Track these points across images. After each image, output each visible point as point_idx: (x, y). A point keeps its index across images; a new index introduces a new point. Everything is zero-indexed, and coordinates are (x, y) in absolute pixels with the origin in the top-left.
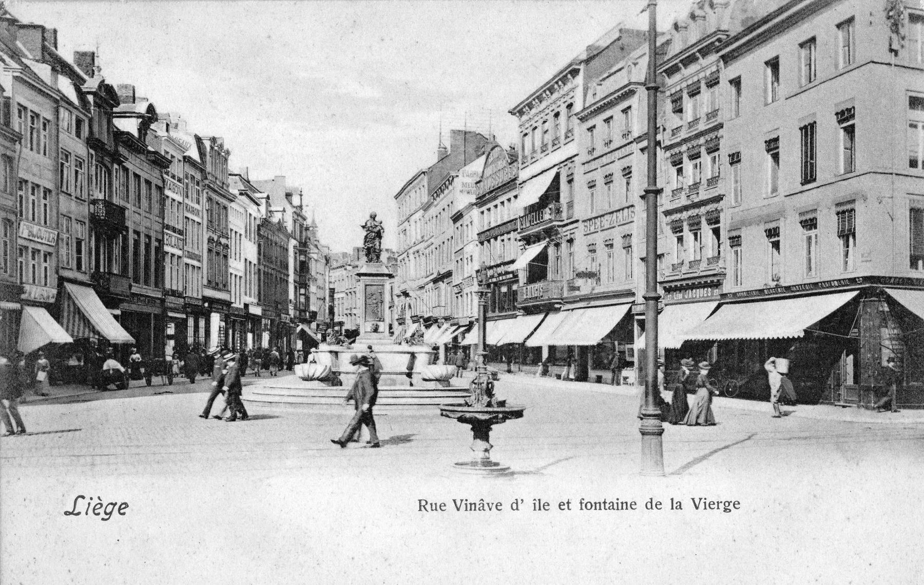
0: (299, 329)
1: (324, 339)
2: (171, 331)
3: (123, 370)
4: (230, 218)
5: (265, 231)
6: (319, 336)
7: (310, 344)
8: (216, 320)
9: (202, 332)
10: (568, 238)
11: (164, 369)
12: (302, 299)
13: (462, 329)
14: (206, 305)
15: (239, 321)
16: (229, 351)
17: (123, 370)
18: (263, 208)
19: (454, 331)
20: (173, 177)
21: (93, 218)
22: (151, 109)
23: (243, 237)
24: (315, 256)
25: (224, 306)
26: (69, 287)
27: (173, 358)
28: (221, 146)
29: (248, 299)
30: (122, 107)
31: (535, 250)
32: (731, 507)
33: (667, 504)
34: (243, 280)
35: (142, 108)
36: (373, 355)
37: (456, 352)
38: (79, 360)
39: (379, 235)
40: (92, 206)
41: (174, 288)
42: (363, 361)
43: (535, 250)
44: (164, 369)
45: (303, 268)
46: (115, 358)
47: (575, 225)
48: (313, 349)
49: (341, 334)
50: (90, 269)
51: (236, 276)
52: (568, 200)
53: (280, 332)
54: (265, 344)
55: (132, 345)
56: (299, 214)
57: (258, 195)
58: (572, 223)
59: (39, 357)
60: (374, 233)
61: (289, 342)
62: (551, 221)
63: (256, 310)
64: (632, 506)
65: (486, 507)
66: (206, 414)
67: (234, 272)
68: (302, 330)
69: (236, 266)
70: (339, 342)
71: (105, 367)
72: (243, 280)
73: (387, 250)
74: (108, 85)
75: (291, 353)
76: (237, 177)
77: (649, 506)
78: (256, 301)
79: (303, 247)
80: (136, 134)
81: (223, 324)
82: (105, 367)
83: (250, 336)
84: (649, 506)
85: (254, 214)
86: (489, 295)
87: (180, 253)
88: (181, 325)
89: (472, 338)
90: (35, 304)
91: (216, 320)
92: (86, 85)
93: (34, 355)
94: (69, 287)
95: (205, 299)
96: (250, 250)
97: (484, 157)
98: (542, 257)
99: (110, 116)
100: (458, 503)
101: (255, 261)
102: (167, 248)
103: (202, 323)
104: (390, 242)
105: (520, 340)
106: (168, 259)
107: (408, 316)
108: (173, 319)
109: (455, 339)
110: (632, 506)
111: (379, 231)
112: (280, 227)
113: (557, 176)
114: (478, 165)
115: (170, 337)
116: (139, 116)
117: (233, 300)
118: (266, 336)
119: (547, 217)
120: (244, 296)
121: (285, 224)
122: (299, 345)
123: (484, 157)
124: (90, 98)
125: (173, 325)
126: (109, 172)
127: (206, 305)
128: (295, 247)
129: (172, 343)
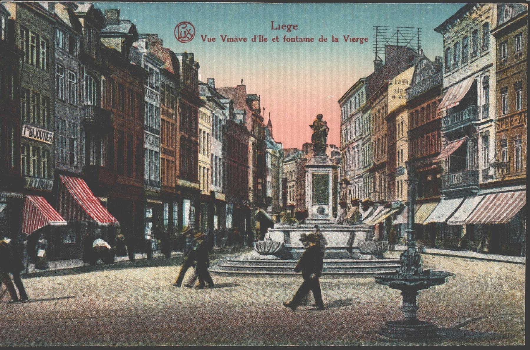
0: (258, 211)
1: (278, 221)
2: (149, 215)
3: (109, 247)
4: (200, 121)
5: (232, 135)
6: (274, 218)
7: (267, 224)
8: (187, 205)
9: (176, 215)
10: (484, 134)
11: (146, 247)
12: (260, 187)
13: (394, 211)
14: (179, 192)
15: (205, 205)
16: (200, 231)
17: (109, 247)
18: (227, 112)
19: (387, 213)
20: (152, 86)
21: (84, 121)
22: (133, 28)
23: (210, 136)
24: (270, 151)
25: (195, 196)
26: (64, 179)
27: (152, 237)
28: (192, 60)
29: (212, 188)
30: (109, 28)
31: (457, 144)
32: (364, 41)
33: (330, 39)
34: (210, 172)
35: (125, 28)
36: (319, 233)
37: (388, 233)
38: (71, 238)
39: (325, 134)
40: (82, 112)
41: (153, 178)
42: (311, 238)
43: (457, 144)
44: (146, 247)
45: (260, 161)
46: (103, 238)
47: (490, 124)
48: (270, 229)
49: (292, 216)
50: (82, 163)
51: (204, 168)
52: (484, 103)
53: (242, 214)
54: (229, 225)
55: (117, 227)
56: (257, 118)
57: (223, 101)
58: (487, 122)
59: (39, 237)
60: (319, 129)
61: (248, 222)
62: (469, 120)
63: (220, 197)
64: (311, 40)
65: (238, 40)
66: (178, 283)
67: (203, 165)
68: (260, 212)
69: (204, 159)
70: (291, 222)
71: (94, 245)
72: (210, 172)
73: (331, 146)
74: (97, 10)
75: (250, 231)
76: (205, 86)
77: (321, 40)
78: (220, 189)
79: (260, 146)
80: (119, 49)
81: (193, 208)
82: (94, 245)
83: (216, 219)
84: (321, 40)
85: (221, 117)
86: (417, 182)
87: (157, 150)
88: (158, 211)
89: (401, 220)
90: (35, 193)
91: (187, 205)
92: (77, 11)
93: (36, 235)
94: (64, 179)
95: (178, 187)
96: (216, 148)
97: (413, 68)
98: (462, 150)
99: (99, 36)
100: (224, 37)
101: (220, 156)
102: (147, 146)
103: (176, 209)
104: (333, 138)
105: (442, 220)
106: (147, 155)
107: (348, 202)
108: (151, 205)
109: (388, 219)
110: (311, 40)
111: (325, 130)
112: (241, 127)
113: (475, 83)
114: (408, 74)
115: (149, 220)
116: (123, 35)
117: (202, 189)
118: (229, 220)
119: (466, 117)
120: (210, 184)
121: (246, 125)
122: (258, 224)
123: (413, 68)
124: (82, 20)
125: (151, 210)
126: (98, 82)
127: (179, 192)
128: (254, 143)
129: (151, 224)
